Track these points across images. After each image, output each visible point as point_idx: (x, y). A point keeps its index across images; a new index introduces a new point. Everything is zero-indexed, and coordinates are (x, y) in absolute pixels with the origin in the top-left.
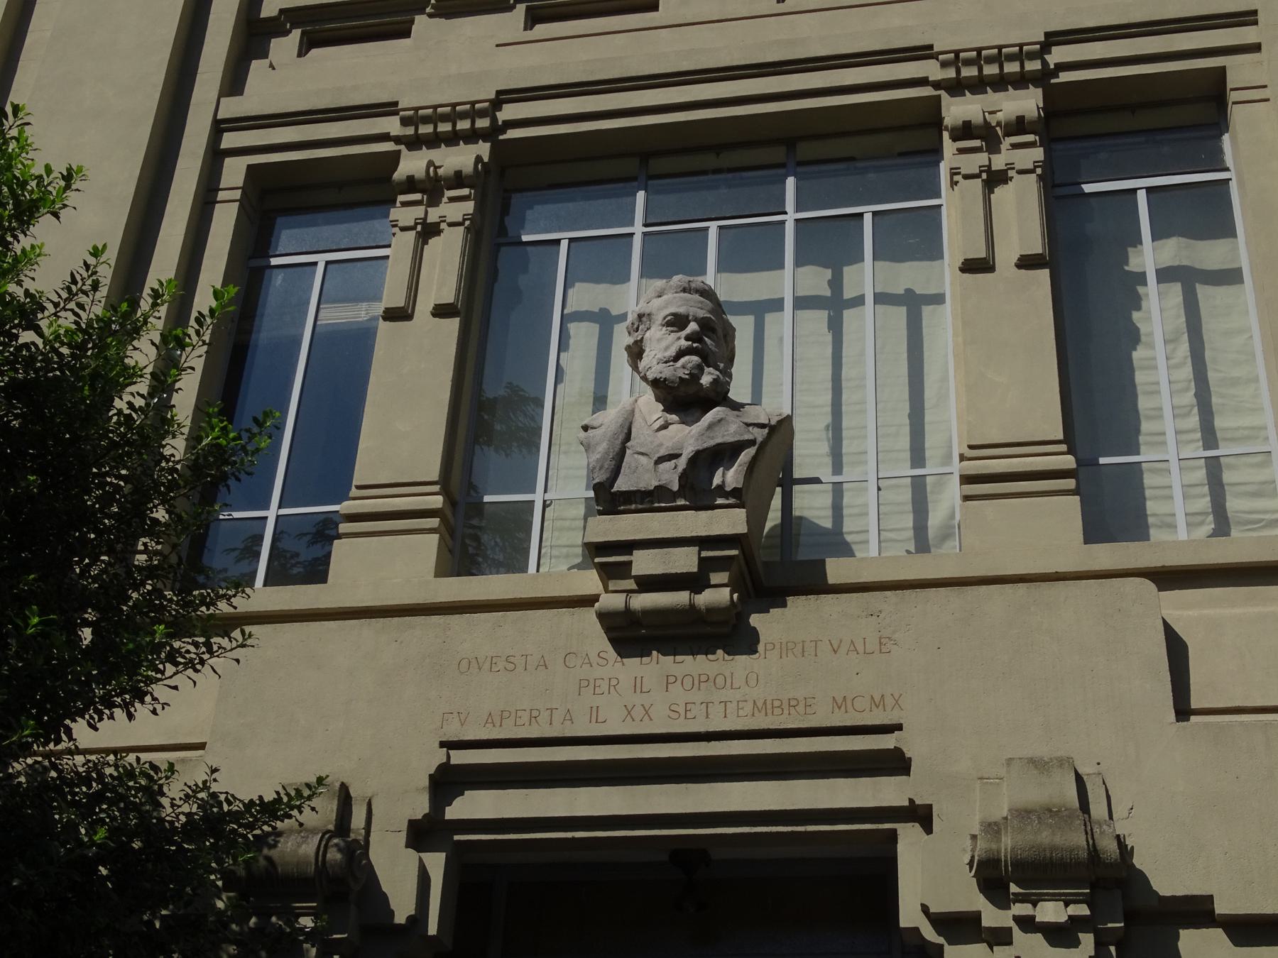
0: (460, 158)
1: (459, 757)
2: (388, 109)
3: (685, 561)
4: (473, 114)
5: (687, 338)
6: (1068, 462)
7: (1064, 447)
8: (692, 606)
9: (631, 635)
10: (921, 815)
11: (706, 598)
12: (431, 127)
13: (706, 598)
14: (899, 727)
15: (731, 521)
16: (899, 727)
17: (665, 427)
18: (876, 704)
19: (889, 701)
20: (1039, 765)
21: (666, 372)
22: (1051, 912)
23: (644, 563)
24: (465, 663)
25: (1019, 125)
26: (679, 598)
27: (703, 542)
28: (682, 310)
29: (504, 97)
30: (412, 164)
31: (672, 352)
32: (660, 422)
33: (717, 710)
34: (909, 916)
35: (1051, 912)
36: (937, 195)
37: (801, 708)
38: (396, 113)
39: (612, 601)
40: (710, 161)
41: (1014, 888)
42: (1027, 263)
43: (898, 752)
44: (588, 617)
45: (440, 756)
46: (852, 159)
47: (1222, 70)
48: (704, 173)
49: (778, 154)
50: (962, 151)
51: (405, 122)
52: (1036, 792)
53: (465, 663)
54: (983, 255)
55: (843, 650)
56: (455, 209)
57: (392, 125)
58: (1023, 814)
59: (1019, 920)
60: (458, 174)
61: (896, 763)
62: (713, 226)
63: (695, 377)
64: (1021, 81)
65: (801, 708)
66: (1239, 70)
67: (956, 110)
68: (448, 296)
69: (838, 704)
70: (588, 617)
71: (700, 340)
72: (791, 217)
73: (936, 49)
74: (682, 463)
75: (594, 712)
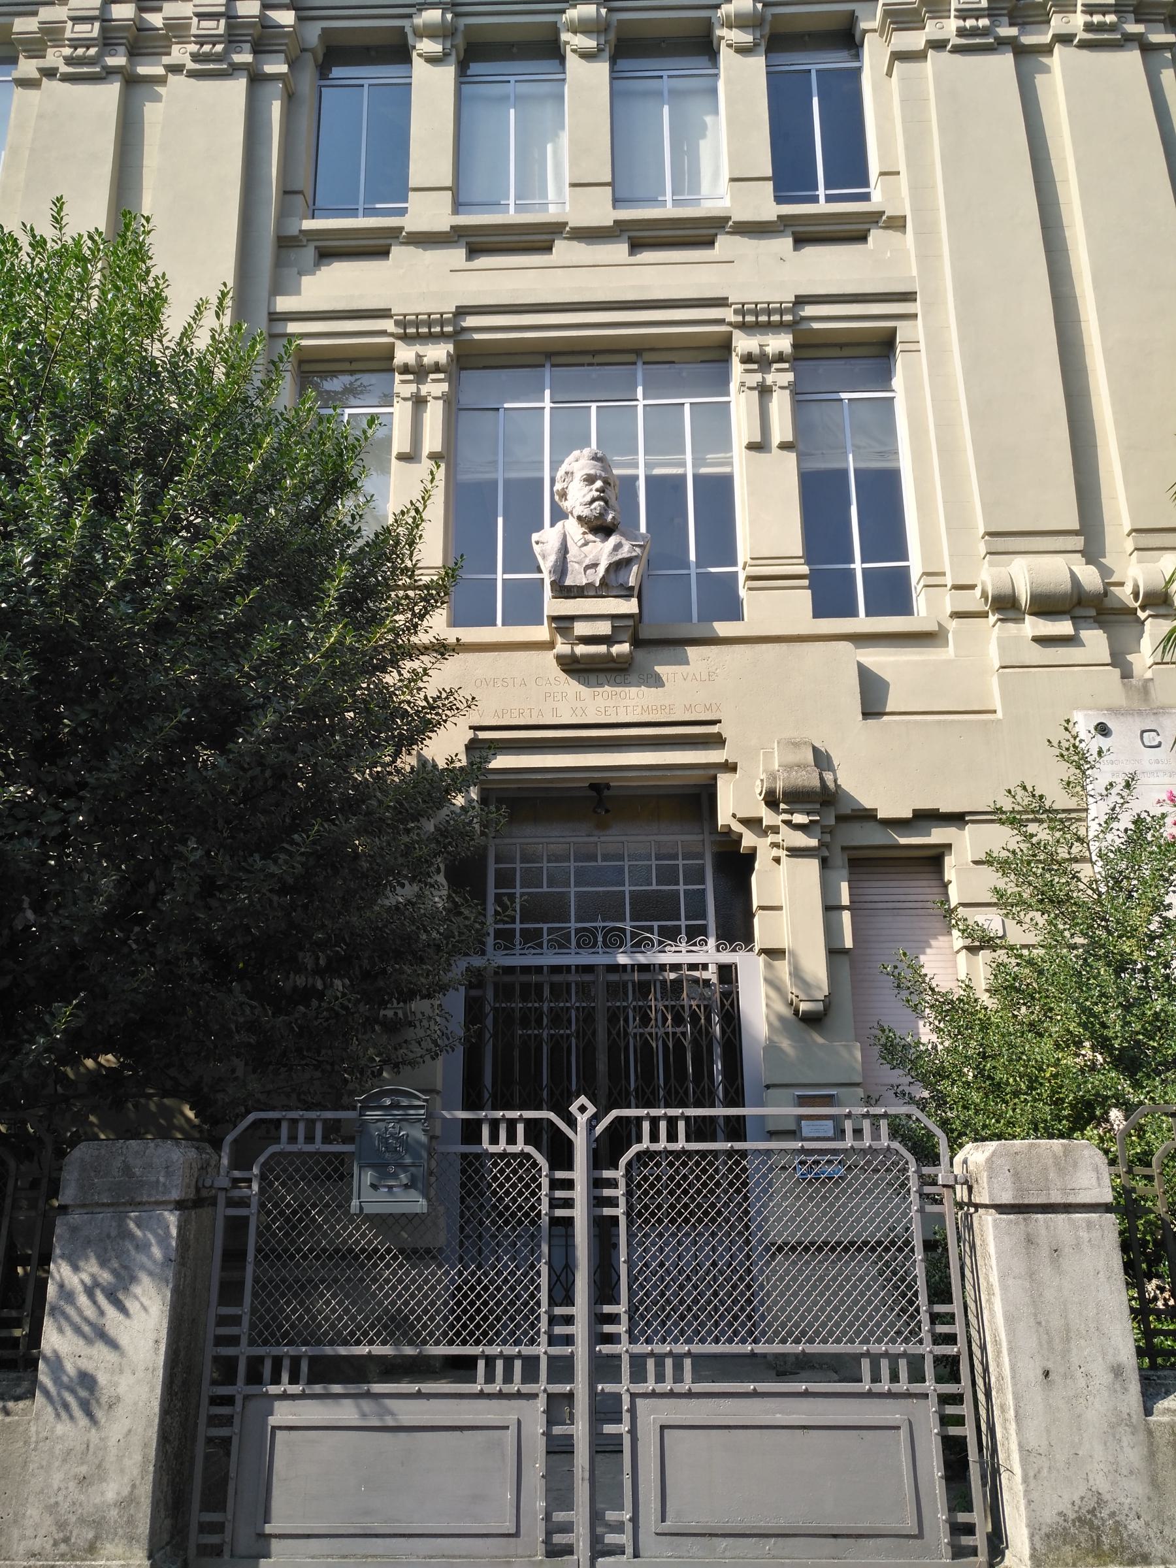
0: (438, 353)
1: (482, 735)
2: (384, 314)
3: (604, 628)
4: (442, 323)
5: (597, 490)
6: (805, 569)
7: (802, 561)
8: (609, 653)
9: (573, 666)
10: (730, 767)
11: (616, 649)
12: (417, 330)
13: (616, 649)
14: (720, 721)
15: (630, 606)
16: (720, 721)
17: (586, 544)
18: (708, 708)
19: (714, 708)
20: (796, 745)
21: (585, 512)
22: (800, 819)
23: (581, 629)
24: (478, 682)
25: (780, 358)
26: (602, 649)
27: (613, 617)
28: (592, 472)
29: (462, 311)
30: (404, 354)
31: (588, 498)
32: (582, 541)
33: (622, 710)
34: (724, 817)
35: (800, 819)
36: (728, 395)
37: (667, 710)
38: (391, 317)
39: (562, 648)
40: (588, 359)
41: (782, 806)
42: (784, 446)
43: (719, 735)
44: (549, 658)
45: (470, 734)
46: (673, 362)
47: (895, 330)
48: (583, 365)
49: (631, 358)
50: (747, 371)
51: (397, 323)
52: (793, 757)
53: (478, 682)
54: (759, 440)
55: (689, 678)
56: (435, 388)
57: (388, 325)
58: (789, 767)
59: (786, 822)
60: (437, 364)
61: (718, 741)
62: (594, 406)
63: (602, 515)
64: (781, 326)
65: (667, 710)
66: (904, 331)
67: (744, 343)
68: (438, 448)
69: (688, 708)
70: (549, 658)
71: (603, 491)
72: (640, 404)
73: (730, 301)
74: (601, 570)
75: (555, 710)
